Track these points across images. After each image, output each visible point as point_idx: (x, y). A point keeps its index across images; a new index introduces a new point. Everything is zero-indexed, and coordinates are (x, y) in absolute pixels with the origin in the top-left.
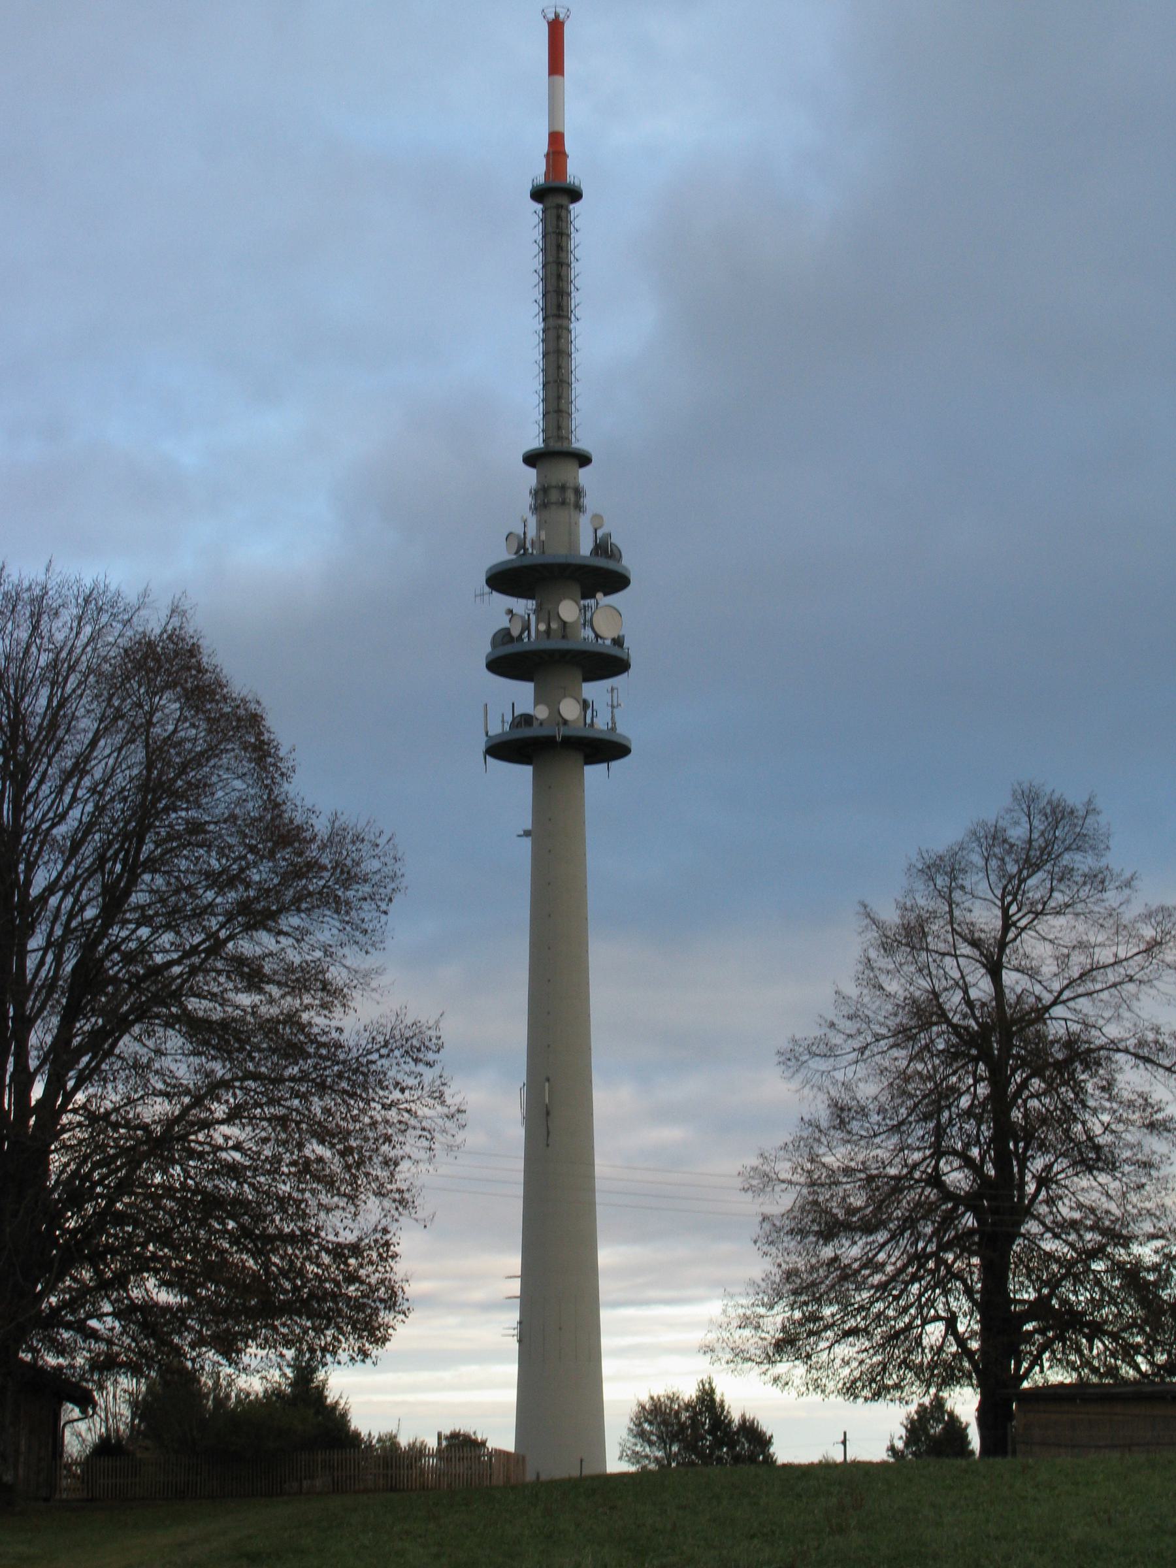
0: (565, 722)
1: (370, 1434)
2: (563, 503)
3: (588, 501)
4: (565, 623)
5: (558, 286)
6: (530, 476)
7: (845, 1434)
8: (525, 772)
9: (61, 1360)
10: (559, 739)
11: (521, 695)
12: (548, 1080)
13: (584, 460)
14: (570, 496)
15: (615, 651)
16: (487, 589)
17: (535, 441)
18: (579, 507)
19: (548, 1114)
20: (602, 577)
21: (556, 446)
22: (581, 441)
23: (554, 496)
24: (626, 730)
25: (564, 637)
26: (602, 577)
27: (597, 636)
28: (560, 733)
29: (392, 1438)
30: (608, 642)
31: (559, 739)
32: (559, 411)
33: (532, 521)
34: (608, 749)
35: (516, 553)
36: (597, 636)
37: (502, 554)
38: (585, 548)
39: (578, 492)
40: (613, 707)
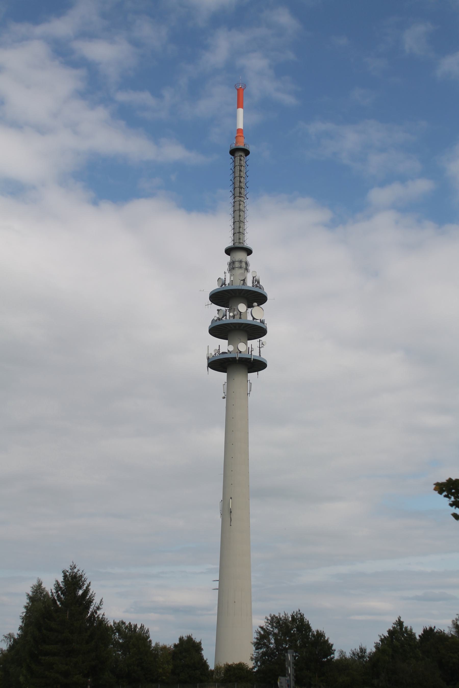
0: (240, 352)
1: (130, 623)
2: (241, 267)
3: (251, 268)
4: (241, 312)
5: (240, 185)
6: (228, 258)
7: (90, 583)
8: (223, 376)
9: (262, 650)
10: (237, 359)
11: (223, 346)
12: (231, 498)
13: (249, 252)
14: (244, 265)
15: (261, 325)
16: (210, 302)
17: (229, 244)
18: (247, 269)
19: (231, 512)
20: (256, 298)
21: (237, 245)
22: (248, 244)
23: (237, 265)
24: (265, 356)
25: (240, 318)
26: (256, 298)
27: (254, 319)
28: (239, 356)
29: (332, 645)
30: (259, 321)
31: (237, 359)
32: (240, 221)
33: (228, 275)
34: (257, 365)
35: (221, 286)
36: (254, 319)
37: (215, 286)
38: (249, 283)
39: (247, 264)
40: (260, 348)
